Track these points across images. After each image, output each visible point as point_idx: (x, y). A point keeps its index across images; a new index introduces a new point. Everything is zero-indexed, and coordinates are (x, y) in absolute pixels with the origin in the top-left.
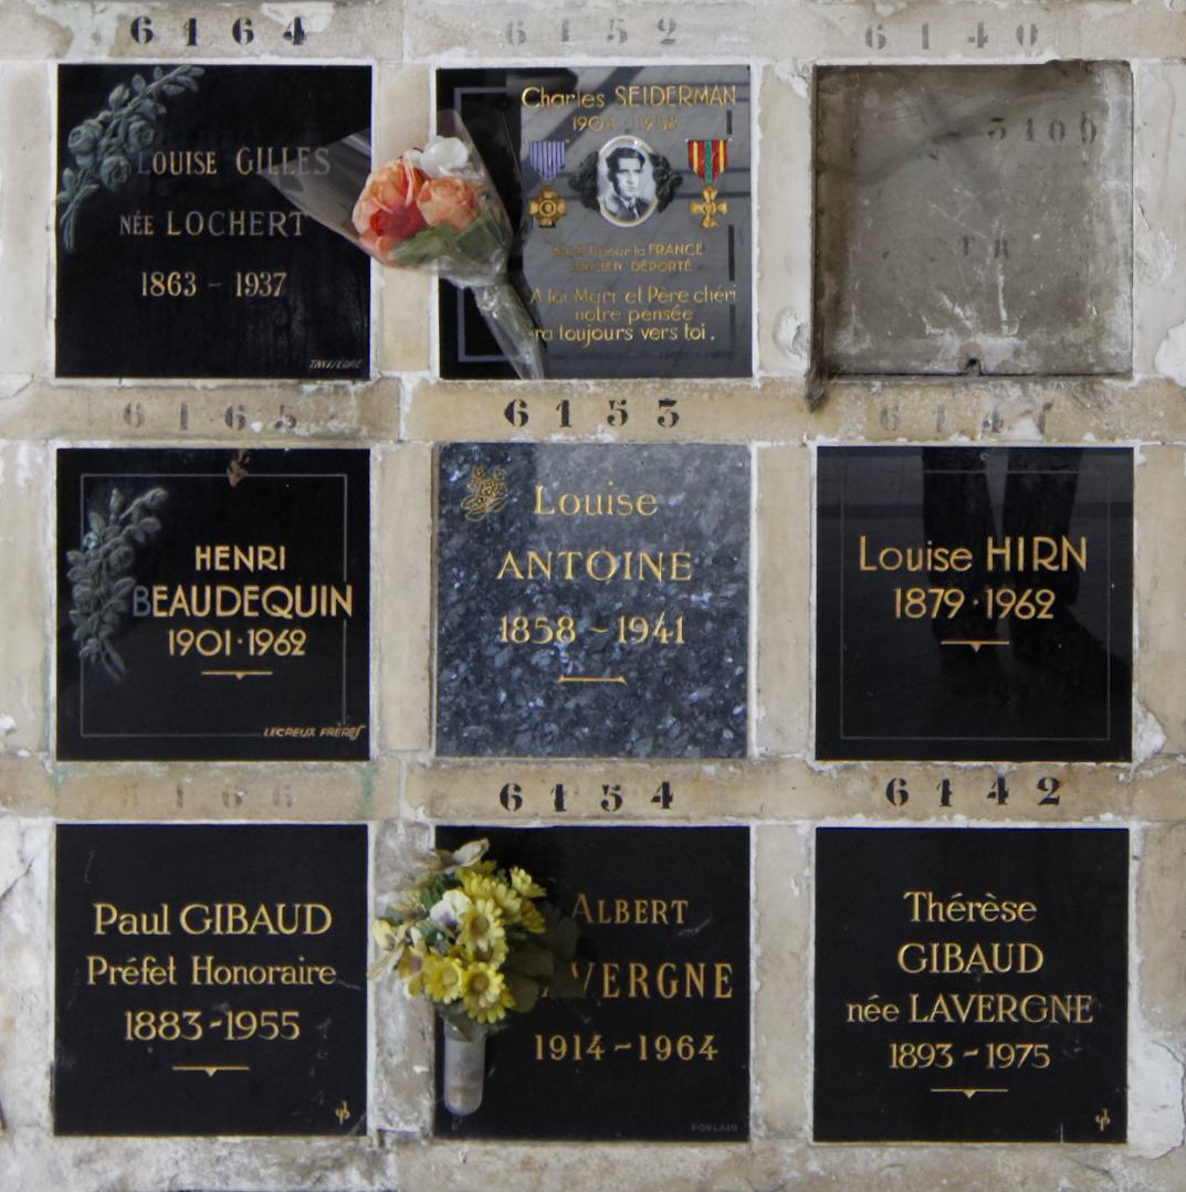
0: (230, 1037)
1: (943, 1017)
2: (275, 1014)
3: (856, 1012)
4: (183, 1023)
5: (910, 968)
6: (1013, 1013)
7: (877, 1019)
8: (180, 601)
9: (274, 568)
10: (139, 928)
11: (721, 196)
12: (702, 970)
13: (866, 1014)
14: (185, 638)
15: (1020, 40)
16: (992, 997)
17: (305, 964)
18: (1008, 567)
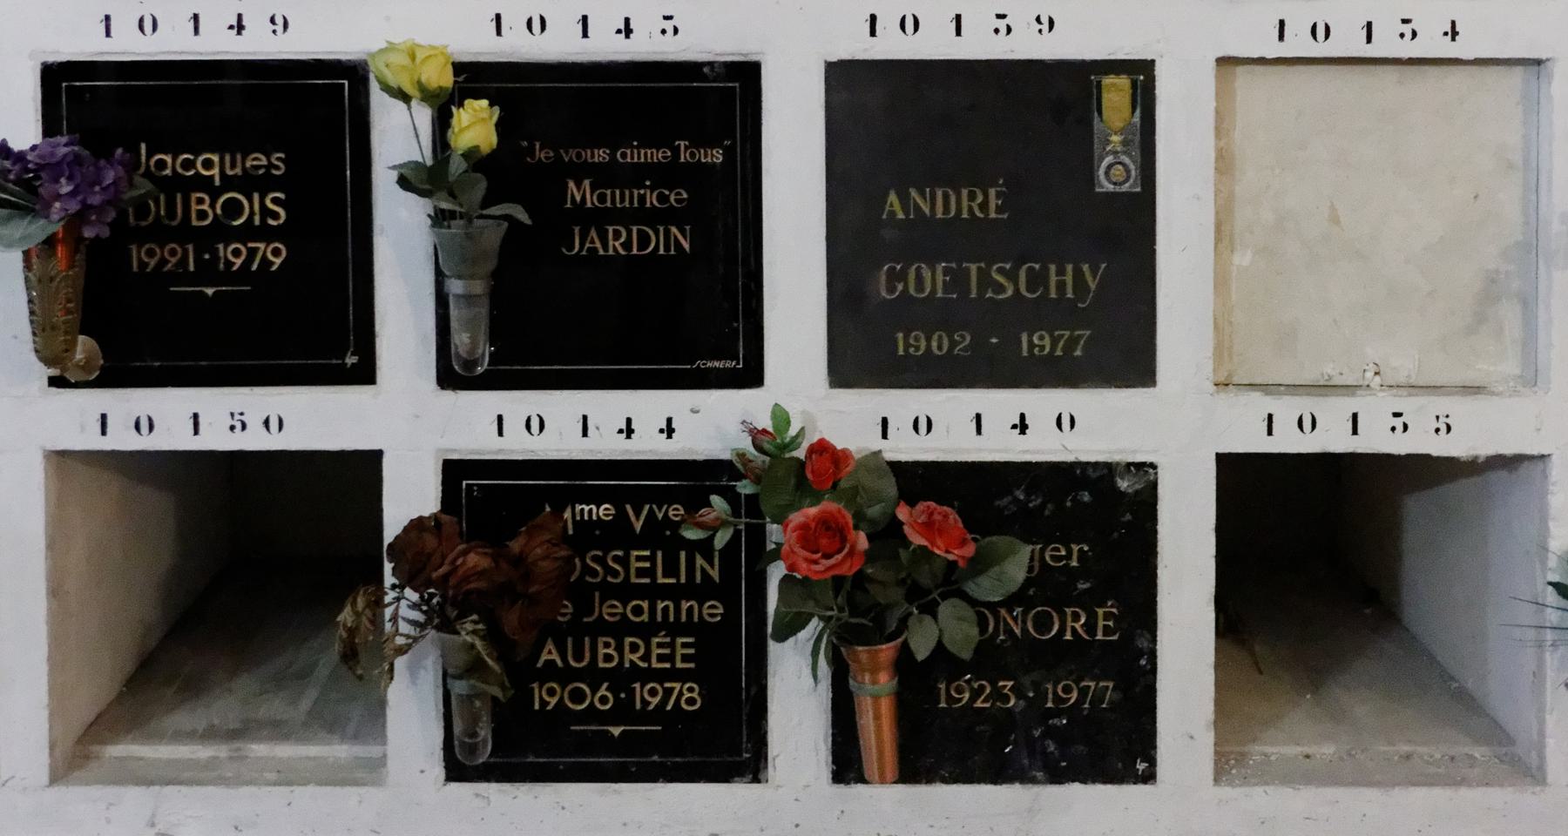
1: (595, 249)
6: (621, 244)
9: (643, 665)
10: (613, 201)
11: (1363, 751)
13: (601, 514)
15: (141, 28)
17: (638, 147)
18: (692, 651)
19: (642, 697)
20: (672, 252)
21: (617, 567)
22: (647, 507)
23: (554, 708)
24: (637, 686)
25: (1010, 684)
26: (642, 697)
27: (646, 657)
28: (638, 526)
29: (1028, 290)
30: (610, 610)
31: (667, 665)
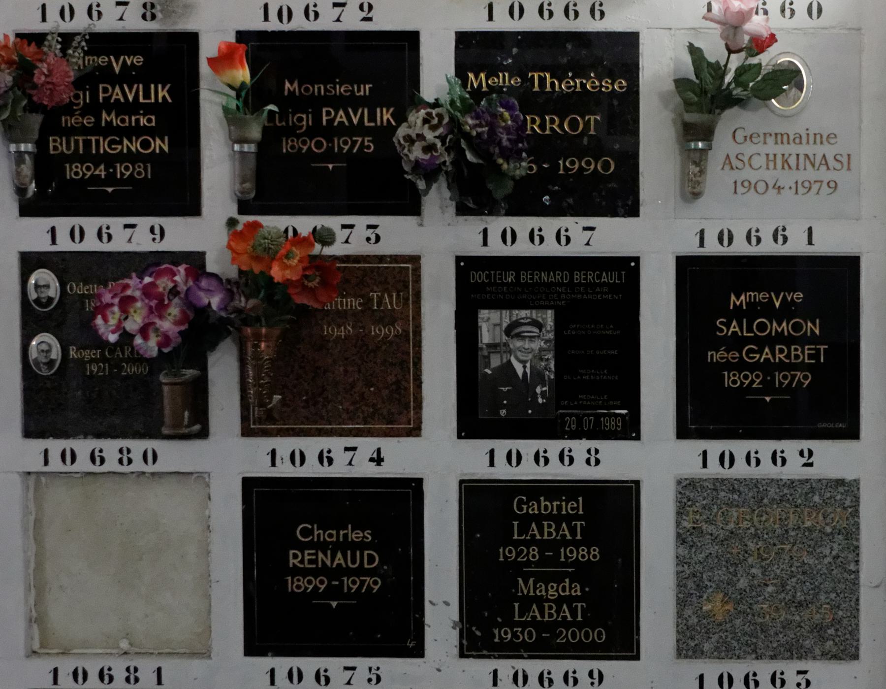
2: (313, 551)
5: (321, 141)
12: (501, 556)
14: (127, 168)
19: (348, 584)
21: (331, 89)
22: (782, 294)
24: (345, 579)
26: (348, 584)
27: (788, 356)
28: (777, 305)
30: (356, 535)
31: (314, 566)
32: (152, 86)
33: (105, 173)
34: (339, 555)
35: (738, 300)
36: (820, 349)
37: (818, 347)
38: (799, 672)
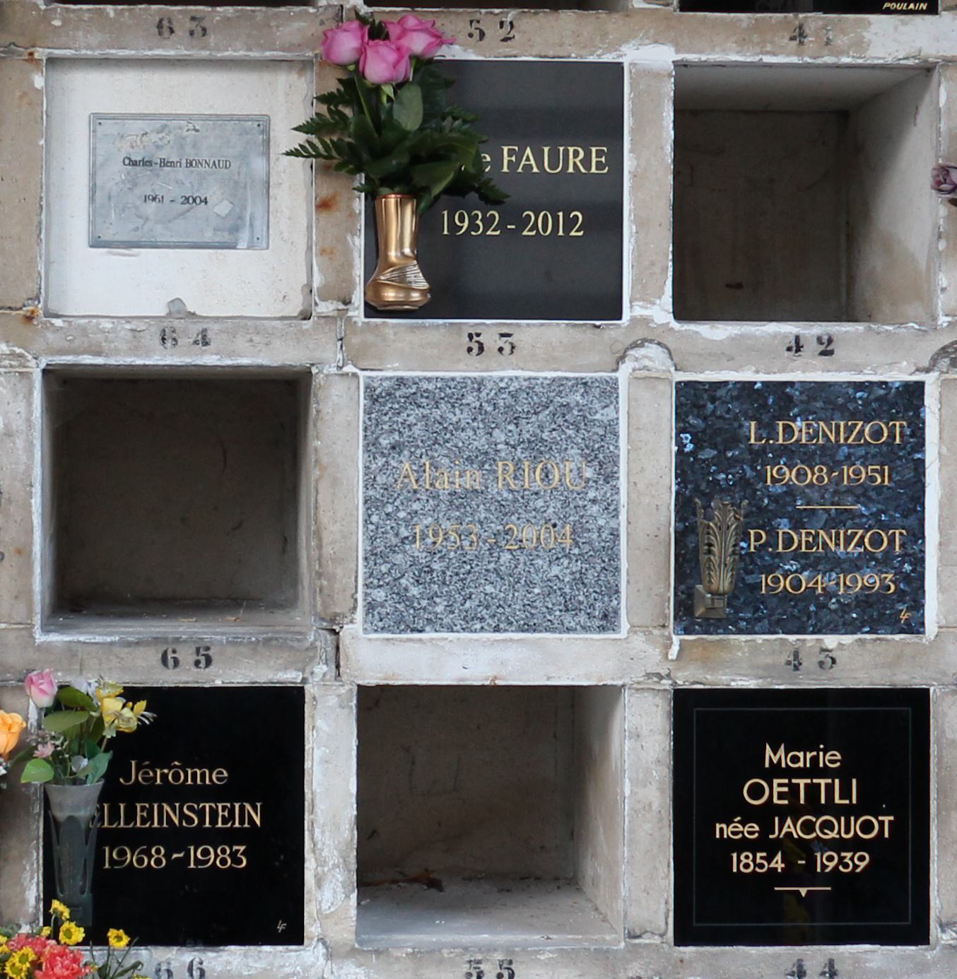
0: (192, 866)
3: (722, 830)
4: (233, 855)
6: (580, 161)
7: (740, 836)
8: (789, 827)
14: (830, 859)
16: (147, 805)
20: (165, 825)
23: (831, 871)
25: (242, 848)
29: (550, 168)
32: (808, 765)
33: (783, 865)
34: (789, 821)
35: (775, 754)
36: (798, 785)
37: (794, 781)
38: (503, 335)
